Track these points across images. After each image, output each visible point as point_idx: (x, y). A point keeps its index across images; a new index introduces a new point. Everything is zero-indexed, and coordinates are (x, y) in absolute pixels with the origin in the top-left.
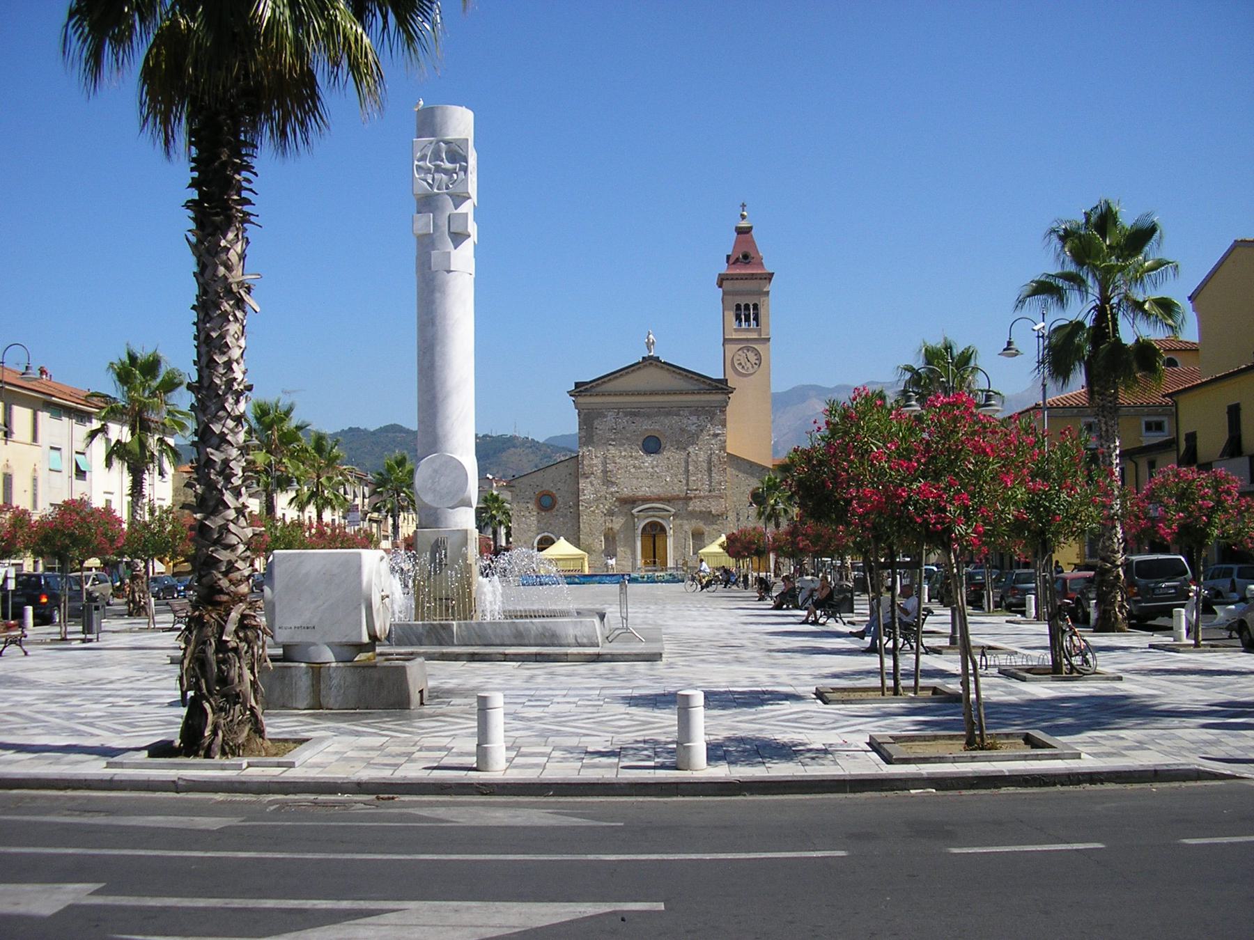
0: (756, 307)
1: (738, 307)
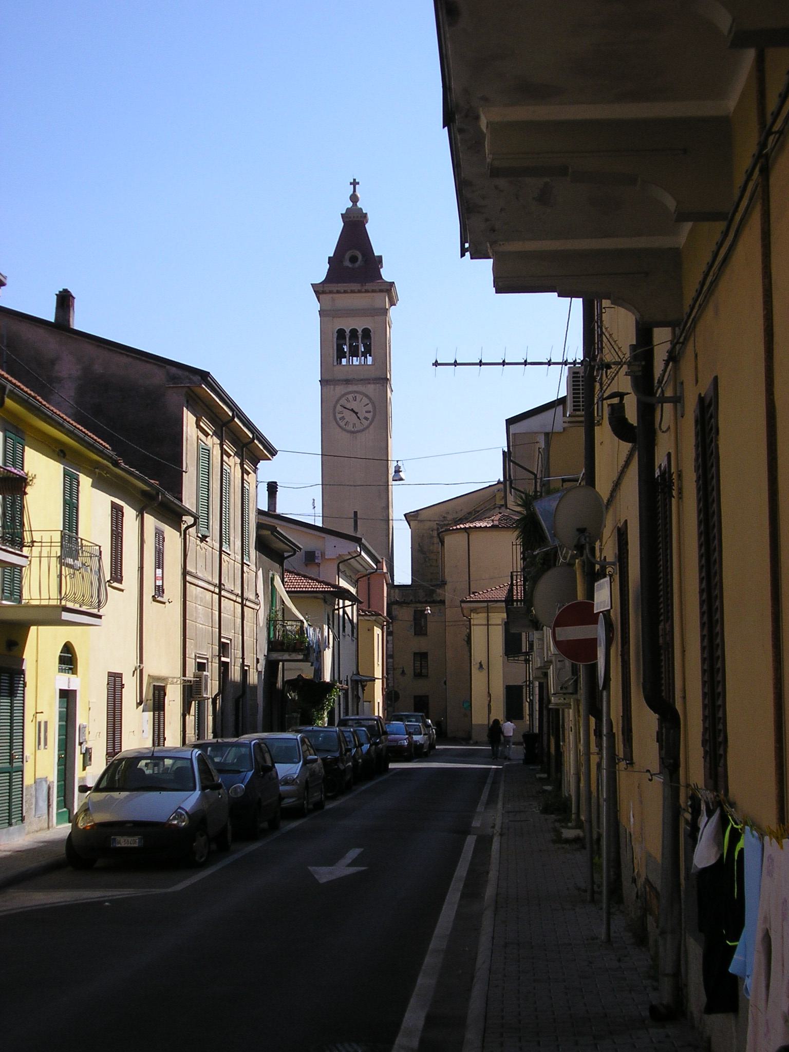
0: (367, 333)
1: (341, 333)
